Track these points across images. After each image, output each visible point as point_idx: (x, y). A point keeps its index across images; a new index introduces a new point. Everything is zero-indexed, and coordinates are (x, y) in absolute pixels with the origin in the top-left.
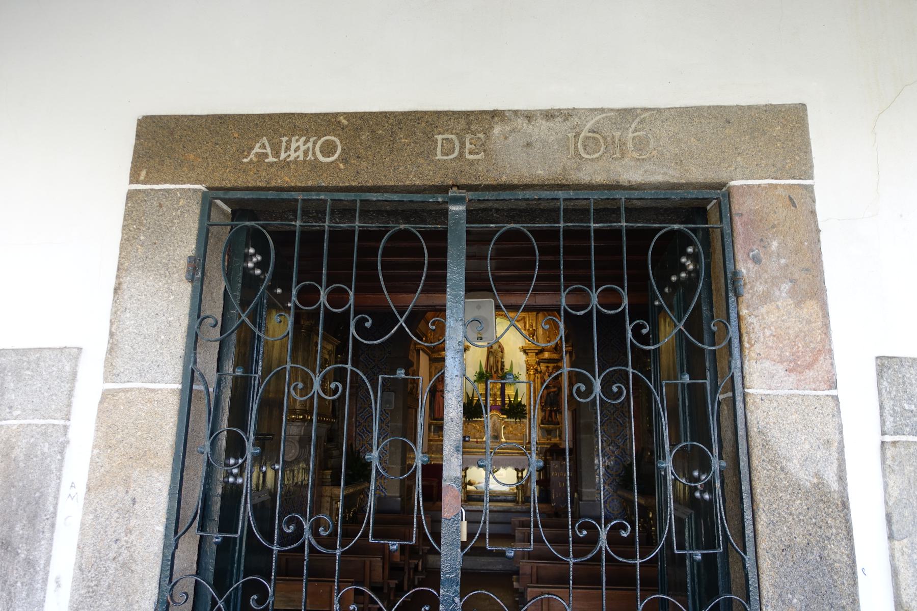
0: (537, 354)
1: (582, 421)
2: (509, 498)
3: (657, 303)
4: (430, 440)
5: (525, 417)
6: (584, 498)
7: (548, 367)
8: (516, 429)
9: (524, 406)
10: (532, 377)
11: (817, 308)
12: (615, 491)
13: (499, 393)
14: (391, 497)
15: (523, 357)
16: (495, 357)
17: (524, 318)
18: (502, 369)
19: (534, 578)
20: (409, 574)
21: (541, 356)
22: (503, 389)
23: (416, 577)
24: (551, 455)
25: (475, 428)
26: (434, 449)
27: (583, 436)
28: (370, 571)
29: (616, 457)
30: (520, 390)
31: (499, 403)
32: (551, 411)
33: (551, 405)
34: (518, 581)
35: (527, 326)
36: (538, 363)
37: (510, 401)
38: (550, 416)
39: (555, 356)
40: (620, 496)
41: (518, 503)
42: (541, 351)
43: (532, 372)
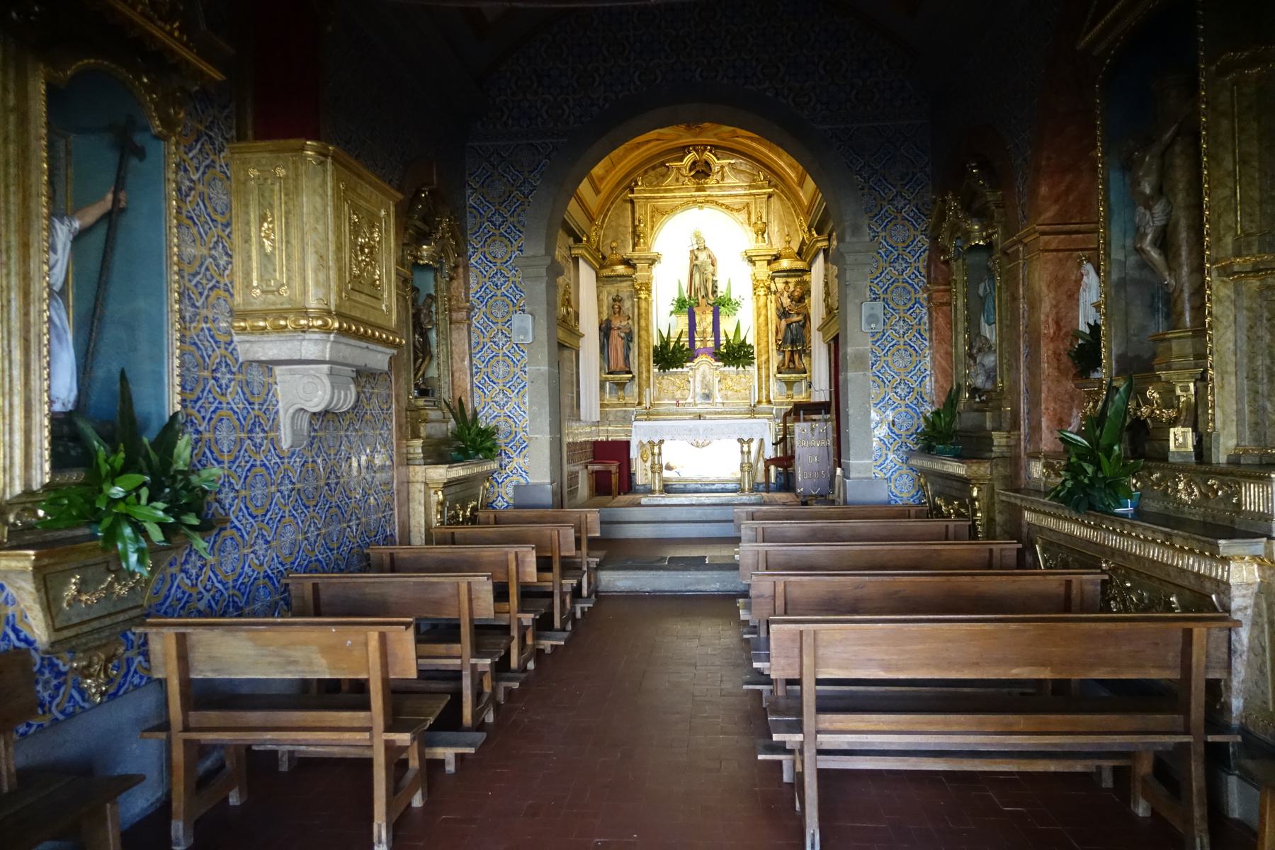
0: (769, 263)
1: (850, 350)
2: (730, 486)
4: (602, 406)
5: (750, 364)
6: (852, 476)
7: (787, 283)
8: (739, 383)
9: (750, 346)
10: (762, 299)
11: (680, 627)
13: (710, 329)
14: (535, 485)
16: (702, 274)
18: (714, 292)
19: (780, 603)
20: (563, 602)
21: (776, 266)
23: (578, 607)
25: (674, 384)
26: (611, 418)
27: (851, 374)
28: (470, 600)
29: (907, 406)
30: (748, 320)
31: (711, 344)
32: (792, 352)
33: (793, 343)
34: (748, 607)
35: (753, 219)
37: (728, 341)
38: (792, 360)
39: (799, 265)
41: (743, 491)
42: (777, 258)
43: (762, 292)
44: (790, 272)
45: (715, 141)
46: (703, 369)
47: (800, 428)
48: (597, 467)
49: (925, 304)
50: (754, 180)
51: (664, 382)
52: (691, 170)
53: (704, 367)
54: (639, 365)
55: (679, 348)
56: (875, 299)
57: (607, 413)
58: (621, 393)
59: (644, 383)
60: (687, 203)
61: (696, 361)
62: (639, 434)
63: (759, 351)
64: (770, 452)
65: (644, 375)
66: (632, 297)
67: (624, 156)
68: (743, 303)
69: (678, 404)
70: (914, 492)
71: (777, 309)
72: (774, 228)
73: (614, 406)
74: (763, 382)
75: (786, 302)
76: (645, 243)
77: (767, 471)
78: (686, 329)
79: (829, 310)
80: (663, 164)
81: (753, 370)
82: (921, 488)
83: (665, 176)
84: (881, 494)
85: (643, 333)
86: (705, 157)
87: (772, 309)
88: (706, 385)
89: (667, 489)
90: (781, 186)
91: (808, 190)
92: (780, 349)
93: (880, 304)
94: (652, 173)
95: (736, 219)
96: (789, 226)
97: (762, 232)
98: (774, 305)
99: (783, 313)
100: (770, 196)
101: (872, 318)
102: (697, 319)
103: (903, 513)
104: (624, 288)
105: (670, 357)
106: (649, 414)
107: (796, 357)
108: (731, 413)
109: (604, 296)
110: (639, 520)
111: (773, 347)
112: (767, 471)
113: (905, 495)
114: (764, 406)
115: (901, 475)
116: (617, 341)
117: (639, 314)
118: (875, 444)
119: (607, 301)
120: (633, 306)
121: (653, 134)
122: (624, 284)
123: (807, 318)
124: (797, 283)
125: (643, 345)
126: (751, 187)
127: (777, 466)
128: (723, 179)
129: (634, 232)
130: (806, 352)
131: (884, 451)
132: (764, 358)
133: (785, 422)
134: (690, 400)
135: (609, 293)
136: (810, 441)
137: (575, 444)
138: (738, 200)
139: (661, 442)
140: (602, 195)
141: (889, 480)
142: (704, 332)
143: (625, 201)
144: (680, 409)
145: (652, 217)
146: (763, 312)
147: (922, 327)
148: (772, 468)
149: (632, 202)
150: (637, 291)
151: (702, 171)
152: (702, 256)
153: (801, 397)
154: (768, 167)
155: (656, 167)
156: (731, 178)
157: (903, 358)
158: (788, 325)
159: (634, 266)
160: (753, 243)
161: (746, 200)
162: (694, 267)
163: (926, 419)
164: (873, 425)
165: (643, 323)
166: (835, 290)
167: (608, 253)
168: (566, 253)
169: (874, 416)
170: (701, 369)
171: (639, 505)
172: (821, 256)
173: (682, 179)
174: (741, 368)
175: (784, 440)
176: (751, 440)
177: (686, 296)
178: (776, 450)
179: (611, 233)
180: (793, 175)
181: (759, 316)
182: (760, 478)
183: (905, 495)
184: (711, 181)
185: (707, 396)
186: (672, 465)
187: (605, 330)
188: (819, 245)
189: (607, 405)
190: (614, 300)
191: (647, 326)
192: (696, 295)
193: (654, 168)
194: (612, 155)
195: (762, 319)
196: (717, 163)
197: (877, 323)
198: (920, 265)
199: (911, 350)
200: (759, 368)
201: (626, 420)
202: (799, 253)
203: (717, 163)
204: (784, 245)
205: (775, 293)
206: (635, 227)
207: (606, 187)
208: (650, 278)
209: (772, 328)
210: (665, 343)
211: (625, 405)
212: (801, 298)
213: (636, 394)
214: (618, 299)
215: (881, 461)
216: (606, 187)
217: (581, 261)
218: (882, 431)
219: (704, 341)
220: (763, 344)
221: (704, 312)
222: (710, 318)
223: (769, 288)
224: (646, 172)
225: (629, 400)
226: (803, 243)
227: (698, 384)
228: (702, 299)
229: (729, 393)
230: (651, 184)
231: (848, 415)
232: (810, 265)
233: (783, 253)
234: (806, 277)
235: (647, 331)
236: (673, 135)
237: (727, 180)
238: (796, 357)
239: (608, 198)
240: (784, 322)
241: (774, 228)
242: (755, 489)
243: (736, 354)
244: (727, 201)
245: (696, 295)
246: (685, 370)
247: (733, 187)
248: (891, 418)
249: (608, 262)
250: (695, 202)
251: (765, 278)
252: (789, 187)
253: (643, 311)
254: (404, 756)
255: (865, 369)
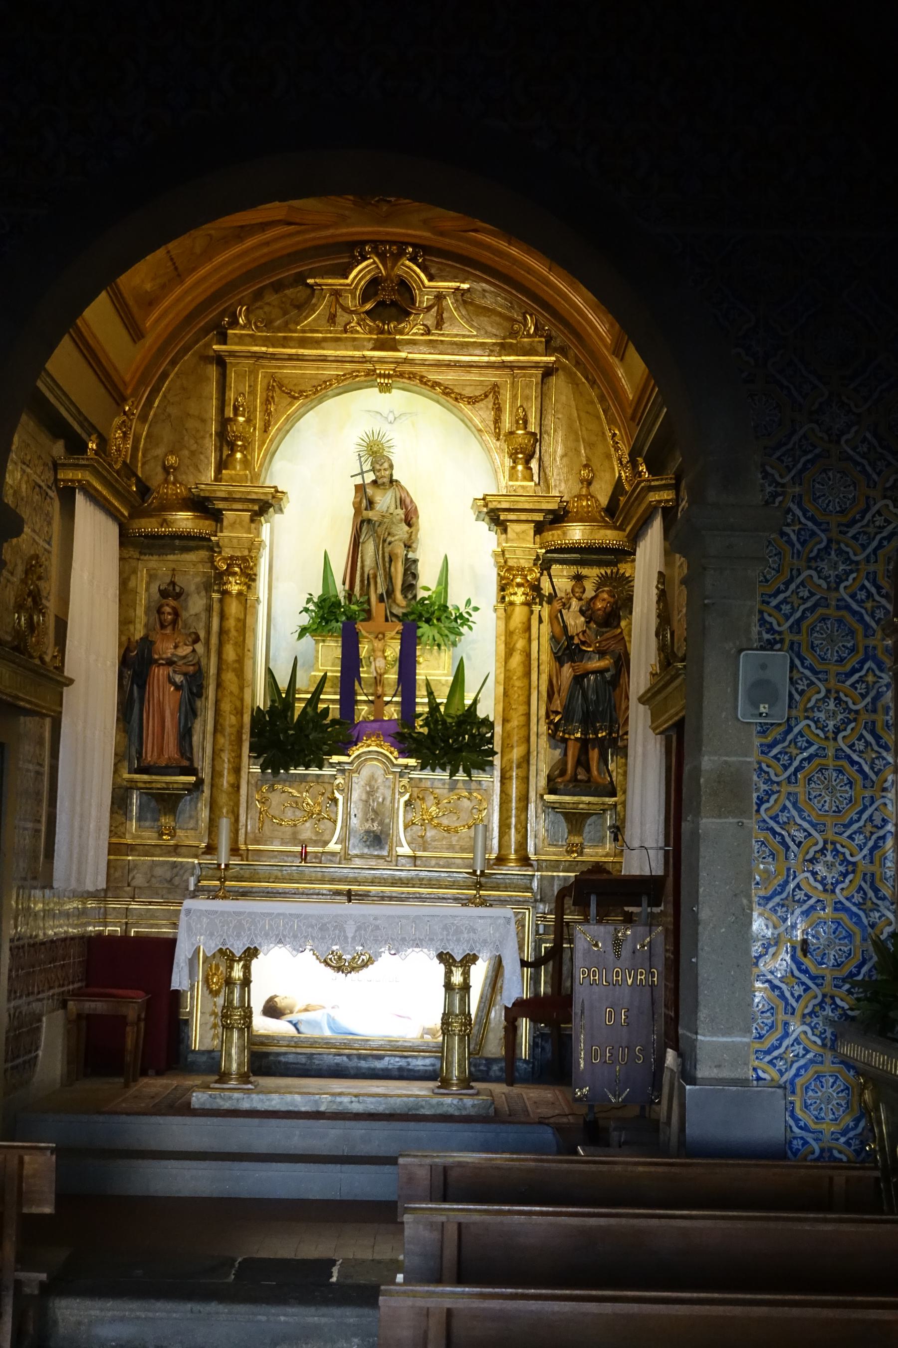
0: (539, 528)
1: (707, 762)
2: (420, 1063)
3: (400, 1278)
4: (114, 849)
5: (485, 765)
6: (702, 1072)
7: (578, 578)
8: (454, 811)
9: (487, 723)
10: (519, 614)
12: (831, 1044)
13: (392, 676)
15: (486, 539)
16: (383, 542)
17: (495, 389)
18: (409, 587)
21: (554, 537)
22: (407, 664)
24: (582, 904)
25: (297, 804)
26: (139, 880)
27: (707, 823)
29: (839, 907)
30: (478, 662)
31: (392, 712)
32: (584, 744)
33: (588, 722)
35: (507, 423)
36: (545, 565)
37: (434, 707)
38: (583, 762)
39: (609, 537)
40: (847, 1063)
41: (446, 1083)
42: (558, 517)
44: (584, 555)
45: (424, 235)
46: (370, 772)
47: (590, 938)
48: (97, 1006)
49: (888, 662)
50: (513, 334)
51: (275, 799)
52: (365, 299)
53: (373, 768)
54: (216, 754)
55: (314, 716)
56: (769, 645)
57: (131, 868)
58: (166, 821)
59: (223, 799)
60: (352, 375)
61: (356, 751)
62: (198, 929)
63: (506, 736)
64: (516, 987)
65: (226, 781)
66: (207, 587)
67: (208, 254)
68: (475, 616)
69: (304, 856)
70: (848, 1121)
71: (553, 638)
72: (555, 447)
73: (148, 850)
74: (514, 810)
75: (575, 621)
76: (246, 463)
77: (511, 1029)
78: (334, 672)
79: (667, 655)
80: (300, 280)
81: (491, 780)
82: (865, 1112)
83: (303, 307)
84: (767, 1125)
85: (229, 677)
86: (399, 271)
87: (543, 632)
88: (376, 812)
89: (265, 1061)
90: (574, 351)
91: (630, 373)
92: (556, 737)
93: (780, 658)
94: (272, 298)
95: (466, 422)
96: (590, 445)
97: (525, 453)
98: (545, 628)
99: (566, 650)
100: (548, 372)
101: (762, 690)
102: (364, 650)
103: (814, 1198)
104: (190, 567)
105: (293, 737)
106: (225, 884)
107: (594, 754)
108: (430, 883)
109: (140, 582)
110: (184, 1154)
111: (539, 728)
112: (511, 1029)
113: (828, 1128)
114: (512, 869)
115: (818, 1077)
116: (164, 694)
117: (222, 632)
118: (760, 994)
119: (145, 594)
120: (209, 609)
121: (274, 210)
122: (191, 557)
123: (622, 662)
124: (603, 581)
125: (226, 706)
126: (504, 348)
127: (534, 1020)
128: (439, 324)
129: (222, 434)
130: (616, 744)
131: (781, 1016)
132: (516, 753)
133: (559, 911)
134: (333, 847)
135: (152, 577)
136: (609, 965)
137: (37, 946)
138: (474, 376)
139: (251, 953)
140: (148, 341)
141: (789, 1087)
142: (378, 681)
143: (206, 359)
144: (308, 869)
145: (267, 401)
146: (520, 644)
147: (880, 718)
148: (525, 1025)
149: (220, 361)
150: (220, 577)
151: (390, 305)
152: (385, 501)
153: (598, 852)
154: (545, 305)
155: (281, 288)
156: (457, 327)
157: (832, 791)
158: (578, 679)
159: (216, 516)
160: (504, 481)
161: (491, 377)
162: (364, 525)
163: (879, 945)
164: (756, 948)
165: (230, 653)
166: (680, 617)
167: (156, 479)
168: (44, 478)
169: (758, 925)
170: (366, 772)
171: (187, 1110)
172: (656, 528)
173: (342, 318)
174: (461, 776)
175: (553, 958)
176: (470, 960)
177: (340, 589)
178: (535, 980)
179: (166, 434)
180: (601, 329)
181: (509, 652)
182: (494, 1047)
183: (828, 1128)
184: (413, 329)
185: (377, 839)
186: (281, 1002)
187: (136, 665)
188: (654, 497)
189: (131, 849)
190: (164, 594)
191: (240, 660)
192: (365, 591)
193: (278, 287)
194: (170, 246)
195: (517, 660)
196: (427, 287)
197: (772, 700)
198: (880, 568)
199: (852, 771)
200: (504, 779)
201: (174, 888)
202: (611, 510)
203: (427, 287)
204: (576, 488)
205: (551, 598)
206: (224, 423)
207: (157, 323)
208: (254, 547)
209: (540, 681)
210: (281, 702)
211: (176, 850)
212: (611, 615)
213: (203, 825)
214: (172, 593)
215: (772, 1040)
216: (157, 323)
217: (80, 500)
218: (779, 963)
219: (377, 702)
220: (516, 721)
221: (380, 636)
222: (393, 649)
223: (536, 588)
224: (258, 295)
225: (185, 837)
226: (619, 484)
227: (356, 808)
228: (379, 598)
229: (430, 833)
230: (269, 325)
231: (696, 922)
232: (635, 537)
233: (574, 507)
234: (624, 568)
235: (240, 673)
236: (325, 216)
237: (448, 329)
238: (594, 754)
239: (162, 351)
240: (567, 671)
241: (555, 447)
242: (478, 1071)
243: (450, 740)
244: (447, 377)
245: (365, 591)
246: (327, 771)
247: (463, 347)
248: (799, 935)
249: (153, 500)
250: (370, 373)
251: (526, 564)
252: (593, 354)
253: (231, 623)
254: (448, 768)
255: (744, 812)
